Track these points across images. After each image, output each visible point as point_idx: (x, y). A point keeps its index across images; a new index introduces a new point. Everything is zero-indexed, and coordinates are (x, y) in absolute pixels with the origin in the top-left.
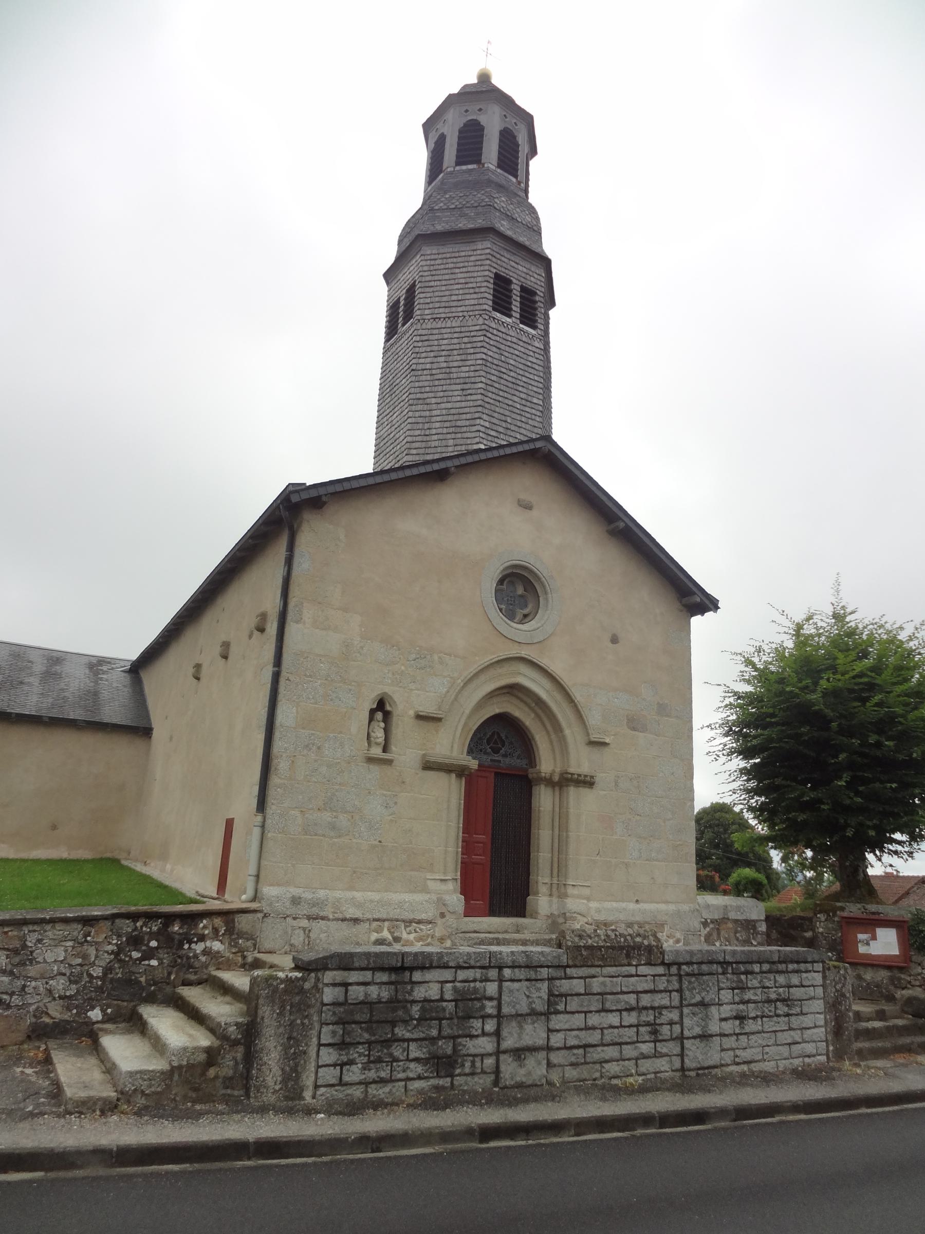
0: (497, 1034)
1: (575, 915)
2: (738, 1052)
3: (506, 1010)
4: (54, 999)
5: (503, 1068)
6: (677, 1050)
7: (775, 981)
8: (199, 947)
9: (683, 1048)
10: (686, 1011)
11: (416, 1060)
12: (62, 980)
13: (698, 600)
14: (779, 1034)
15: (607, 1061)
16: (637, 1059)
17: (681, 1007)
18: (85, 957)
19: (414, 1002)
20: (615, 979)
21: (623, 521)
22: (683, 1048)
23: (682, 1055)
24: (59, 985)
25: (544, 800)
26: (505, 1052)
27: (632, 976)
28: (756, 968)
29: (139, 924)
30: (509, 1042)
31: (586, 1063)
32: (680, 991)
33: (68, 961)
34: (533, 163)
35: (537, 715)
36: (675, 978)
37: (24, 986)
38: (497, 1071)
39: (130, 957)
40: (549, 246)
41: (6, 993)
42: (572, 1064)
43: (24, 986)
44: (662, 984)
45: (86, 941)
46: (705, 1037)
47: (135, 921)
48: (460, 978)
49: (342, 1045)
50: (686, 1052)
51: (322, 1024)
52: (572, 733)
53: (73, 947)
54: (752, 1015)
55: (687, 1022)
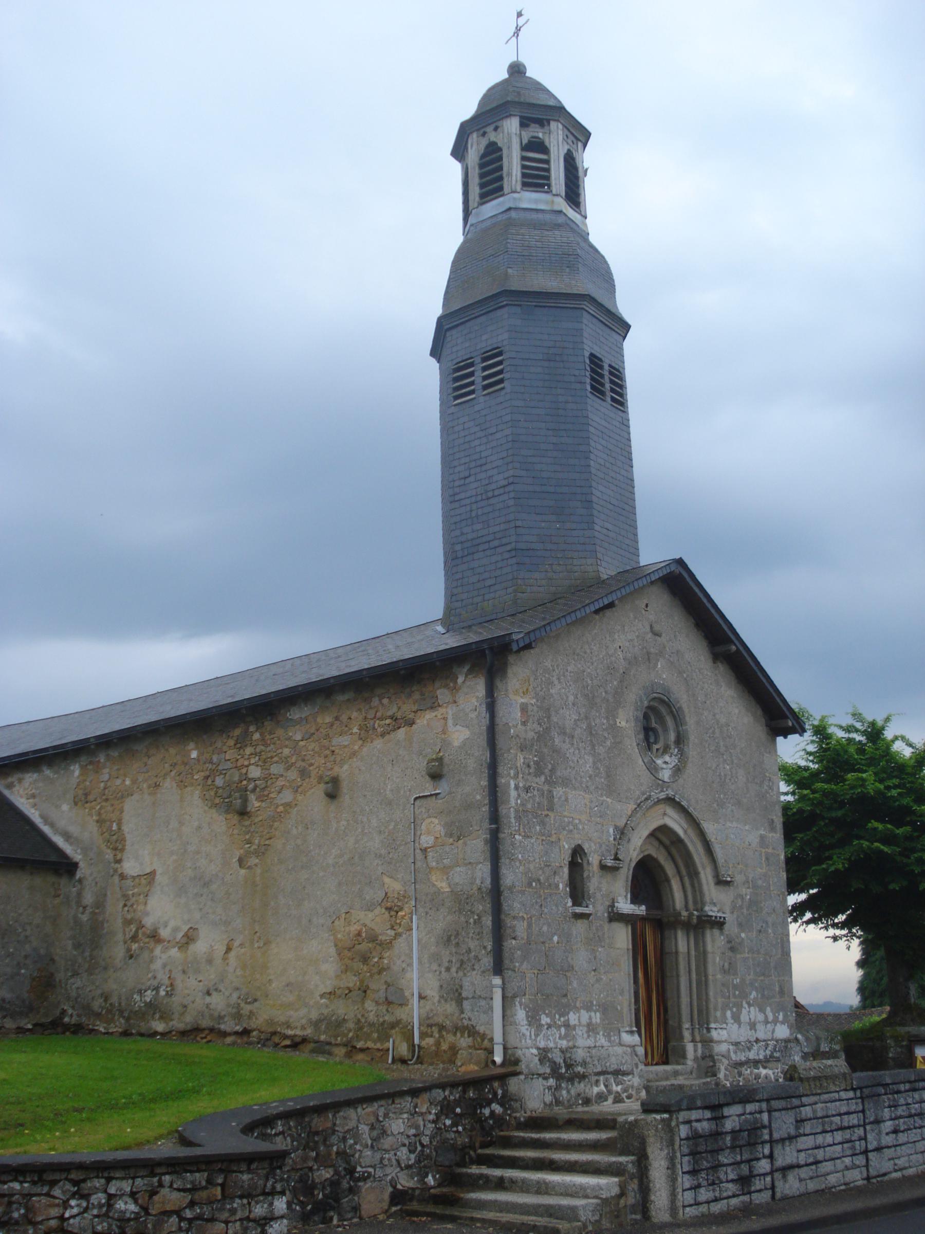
0: (771, 1157)
1: (720, 1057)
2: (897, 1161)
3: (776, 1136)
4: (402, 1169)
5: (777, 1183)
6: (864, 1162)
7: (913, 1098)
8: (487, 1112)
9: (867, 1160)
10: (868, 1127)
11: (732, 1181)
12: (405, 1150)
13: (790, 724)
14: (917, 1144)
15: (828, 1174)
16: (843, 1171)
17: (864, 1126)
18: (417, 1127)
19: (727, 1133)
20: (829, 1105)
21: (735, 645)
22: (867, 1160)
23: (867, 1166)
24: (403, 1153)
25: (682, 942)
26: (777, 1170)
27: (835, 1101)
28: (902, 1087)
29: (447, 1093)
30: (779, 1163)
31: (818, 1176)
32: (863, 1111)
33: (406, 1132)
34: (586, 179)
35: (670, 854)
36: (860, 1101)
37: (382, 1159)
38: (773, 1188)
39: (444, 1124)
40: (625, 306)
41: (371, 1166)
42: (811, 1178)
43: (382, 1159)
44: (853, 1108)
45: (416, 1112)
46: (878, 1149)
47: (444, 1091)
48: (748, 1111)
49: (693, 1172)
50: (871, 1163)
51: (683, 1156)
52: (706, 876)
53: (408, 1119)
54: (902, 1129)
55: (870, 1137)
